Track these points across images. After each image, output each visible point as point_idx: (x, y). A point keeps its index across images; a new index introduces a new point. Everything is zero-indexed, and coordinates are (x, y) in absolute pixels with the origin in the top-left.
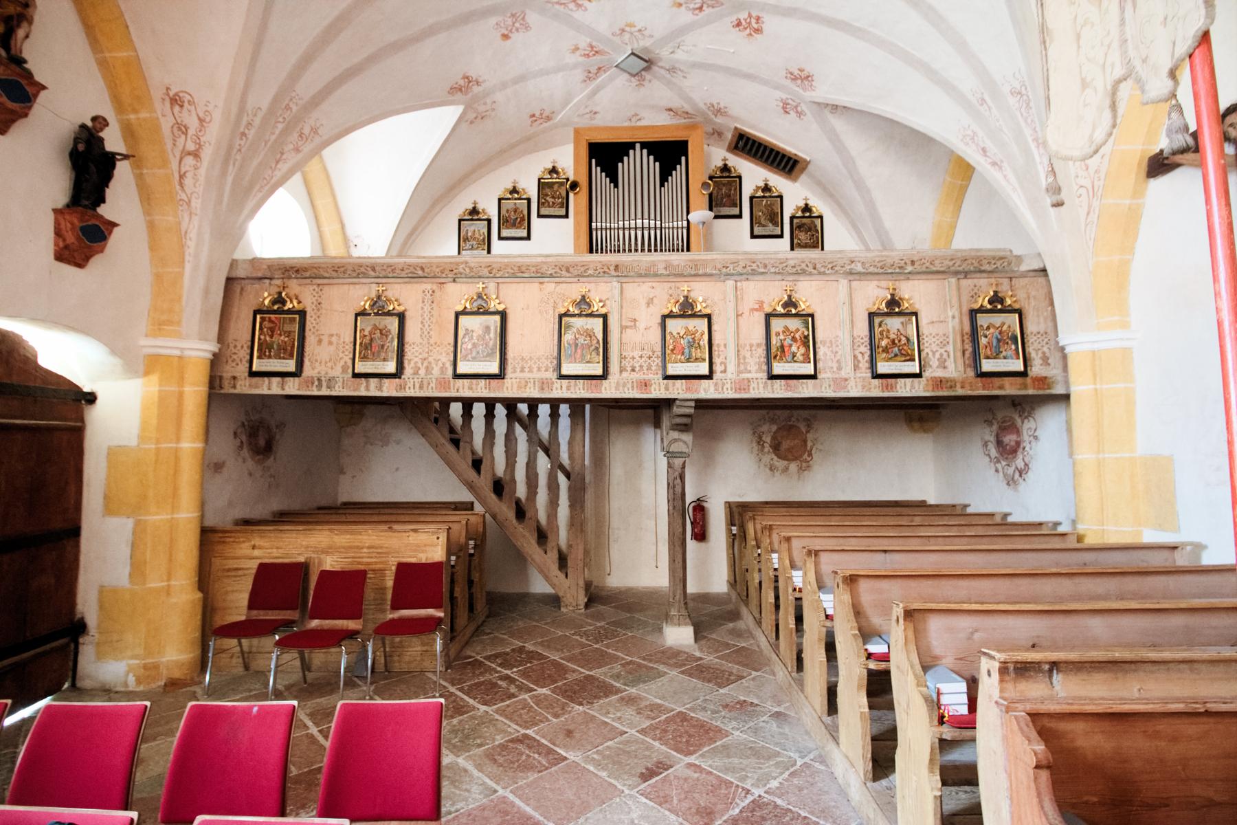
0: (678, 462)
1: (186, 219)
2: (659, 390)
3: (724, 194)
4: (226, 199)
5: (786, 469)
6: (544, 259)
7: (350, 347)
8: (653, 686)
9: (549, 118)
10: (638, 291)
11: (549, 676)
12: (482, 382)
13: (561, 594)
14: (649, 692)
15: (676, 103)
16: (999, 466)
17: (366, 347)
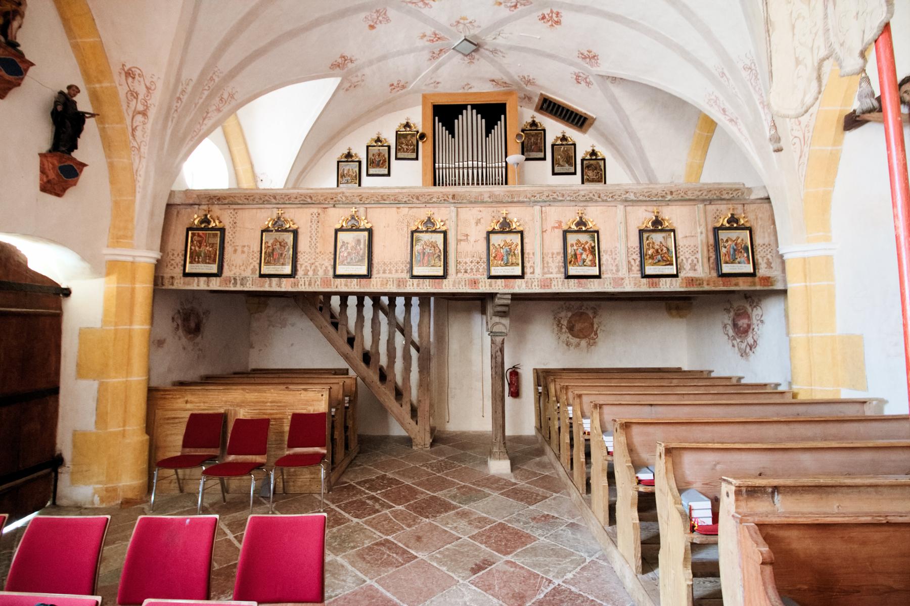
0: (499, 339)
1: (137, 161)
2: (485, 287)
3: (532, 142)
4: (166, 146)
5: (578, 345)
6: (400, 191)
7: (257, 255)
8: (481, 504)
9: (404, 87)
10: (469, 214)
11: (404, 496)
12: (355, 281)
13: (412, 436)
14: (477, 509)
15: (498, 76)
16: (735, 342)
17: (269, 255)
